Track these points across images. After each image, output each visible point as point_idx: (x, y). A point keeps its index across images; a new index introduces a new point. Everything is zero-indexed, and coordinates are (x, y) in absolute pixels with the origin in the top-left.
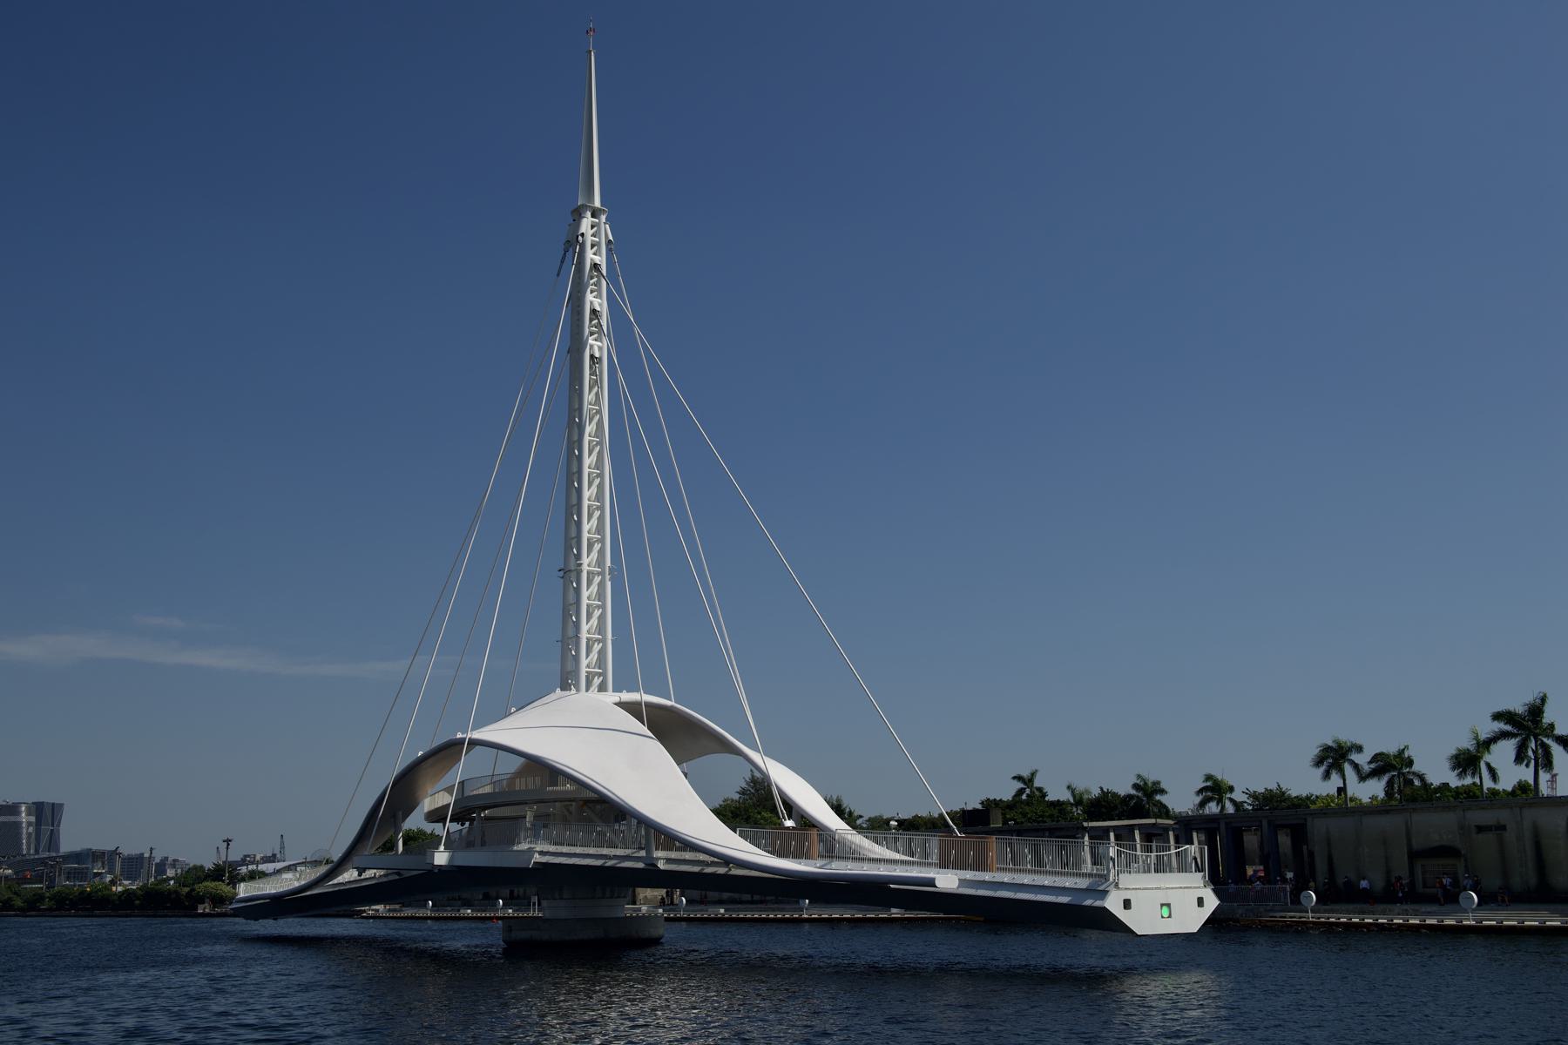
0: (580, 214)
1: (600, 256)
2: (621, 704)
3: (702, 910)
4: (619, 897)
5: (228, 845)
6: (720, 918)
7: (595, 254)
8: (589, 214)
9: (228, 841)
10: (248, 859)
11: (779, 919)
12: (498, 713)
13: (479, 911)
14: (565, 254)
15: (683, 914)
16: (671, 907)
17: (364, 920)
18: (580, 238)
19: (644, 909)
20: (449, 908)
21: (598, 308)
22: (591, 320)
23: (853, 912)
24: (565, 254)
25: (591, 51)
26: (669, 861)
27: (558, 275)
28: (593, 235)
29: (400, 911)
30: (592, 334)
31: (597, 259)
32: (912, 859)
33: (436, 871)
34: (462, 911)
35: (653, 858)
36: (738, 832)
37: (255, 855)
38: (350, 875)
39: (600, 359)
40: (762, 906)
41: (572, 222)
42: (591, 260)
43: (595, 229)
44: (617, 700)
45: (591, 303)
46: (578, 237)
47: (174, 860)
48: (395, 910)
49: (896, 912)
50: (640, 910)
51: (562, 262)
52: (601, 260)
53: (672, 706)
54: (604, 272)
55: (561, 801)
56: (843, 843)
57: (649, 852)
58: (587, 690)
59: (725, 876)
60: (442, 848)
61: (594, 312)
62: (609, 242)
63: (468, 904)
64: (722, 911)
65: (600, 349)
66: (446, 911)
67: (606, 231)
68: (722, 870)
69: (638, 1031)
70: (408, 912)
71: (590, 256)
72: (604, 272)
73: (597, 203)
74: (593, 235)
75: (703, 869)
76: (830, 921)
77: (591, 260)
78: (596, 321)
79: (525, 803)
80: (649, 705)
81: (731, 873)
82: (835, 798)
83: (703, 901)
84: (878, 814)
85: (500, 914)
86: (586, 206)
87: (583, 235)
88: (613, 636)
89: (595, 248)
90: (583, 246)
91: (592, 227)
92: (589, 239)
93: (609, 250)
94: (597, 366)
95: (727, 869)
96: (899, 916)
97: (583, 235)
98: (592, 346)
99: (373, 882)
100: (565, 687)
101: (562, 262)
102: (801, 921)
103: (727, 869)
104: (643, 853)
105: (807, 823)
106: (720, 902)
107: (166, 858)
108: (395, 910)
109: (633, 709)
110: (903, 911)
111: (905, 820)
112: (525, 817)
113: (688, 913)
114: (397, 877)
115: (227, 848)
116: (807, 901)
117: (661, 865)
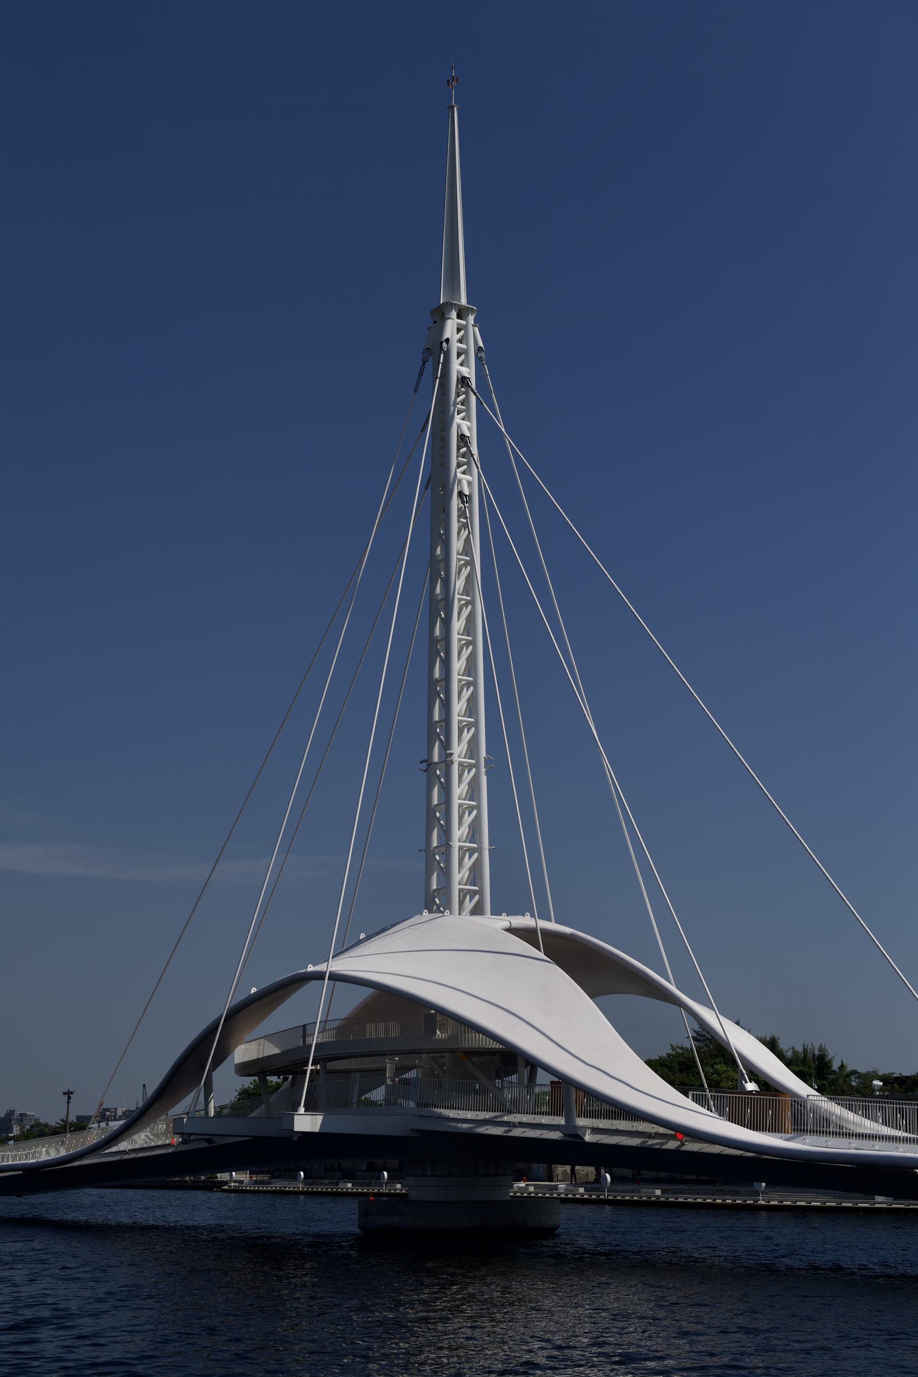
0: (443, 315)
1: (468, 367)
2: (511, 930)
3: (633, 1191)
4: (504, 1175)
5: (69, 1098)
6: (653, 1201)
7: (461, 365)
8: (454, 314)
9: (69, 1094)
10: (108, 1113)
11: (729, 1205)
12: (347, 946)
13: (361, 1185)
14: (424, 364)
15: (605, 1195)
16: (596, 1185)
17: (226, 1194)
18: (444, 344)
19: (562, 1186)
20: (326, 1181)
21: (467, 433)
22: (459, 449)
23: (824, 1199)
24: (424, 364)
25: (454, 106)
26: (595, 1131)
27: (416, 391)
28: (460, 341)
29: (269, 1183)
30: (459, 465)
31: (465, 371)
32: (905, 1134)
33: (296, 1139)
34: (341, 1185)
35: (576, 1127)
36: (690, 1096)
37: (116, 1109)
38: (141, 1139)
39: (470, 497)
40: (710, 1187)
41: (432, 324)
42: (458, 372)
43: (462, 332)
44: (506, 924)
45: (459, 426)
46: (442, 343)
47: (21, 1115)
48: (261, 1183)
49: (881, 1201)
50: (556, 1188)
51: (420, 375)
52: (469, 372)
53: (572, 935)
54: (474, 387)
55: (428, 1052)
56: (815, 1110)
57: (569, 1119)
58: (460, 914)
59: (676, 1152)
60: (302, 1110)
61: (462, 438)
62: (479, 349)
63: (348, 1176)
64: (658, 1192)
65: (470, 484)
66: (322, 1184)
67: (475, 334)
68: (672, 1145)
69: (795, 1345)
70: (277, 1185)
71: (457, 368)
72: (474, 387)
73: (463, 301)
74: (460, 341)
75: (122, 1157)
76: (794, 1210)
77: (458, 372)
78: (465, 449)
79: (383, 1054)
80: (546, 933)
81: (683, 1148)
82: (817, 1046)
83: (636, 1180)
84: (871, 1070)
85: (384, 1190)
86: (452, 304)
87: (447, 340)
88: (490, 845)
89: (463, 357)
90: (447, 354)
91: (459, 330)
92: (455, 346)
93: (478, 360)
94: (467, 505)
95: (678, 1143)
96: (885, 1206)
97: (447, 340)
98: (460, 481)
99: (170, 1150)
100: (430, 906)
101: (420, 375)
102: (756, 1208)
103: (678, 1143)
104: (561, 1121)
105: (768, 1086)
106: (657, 1182)
107: (12, 1112)
108: (261, 1183)
109: (527, 935)
110: (891, 1200)
111: (908, 1077)
112: (385, 1070)
113: (667, 1196)
114: (205, 1145)
115: (68, 1103)
116: (764, 1184)
117: (588, 1138)
